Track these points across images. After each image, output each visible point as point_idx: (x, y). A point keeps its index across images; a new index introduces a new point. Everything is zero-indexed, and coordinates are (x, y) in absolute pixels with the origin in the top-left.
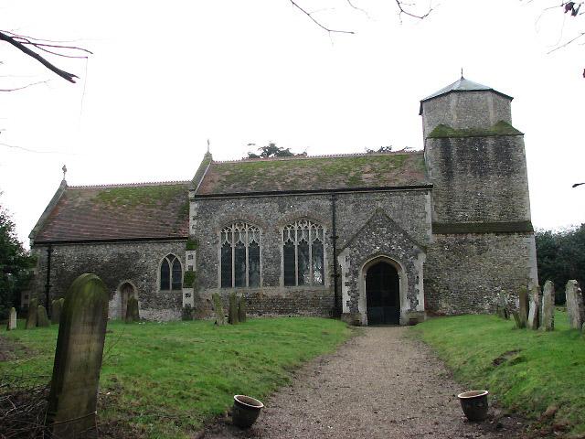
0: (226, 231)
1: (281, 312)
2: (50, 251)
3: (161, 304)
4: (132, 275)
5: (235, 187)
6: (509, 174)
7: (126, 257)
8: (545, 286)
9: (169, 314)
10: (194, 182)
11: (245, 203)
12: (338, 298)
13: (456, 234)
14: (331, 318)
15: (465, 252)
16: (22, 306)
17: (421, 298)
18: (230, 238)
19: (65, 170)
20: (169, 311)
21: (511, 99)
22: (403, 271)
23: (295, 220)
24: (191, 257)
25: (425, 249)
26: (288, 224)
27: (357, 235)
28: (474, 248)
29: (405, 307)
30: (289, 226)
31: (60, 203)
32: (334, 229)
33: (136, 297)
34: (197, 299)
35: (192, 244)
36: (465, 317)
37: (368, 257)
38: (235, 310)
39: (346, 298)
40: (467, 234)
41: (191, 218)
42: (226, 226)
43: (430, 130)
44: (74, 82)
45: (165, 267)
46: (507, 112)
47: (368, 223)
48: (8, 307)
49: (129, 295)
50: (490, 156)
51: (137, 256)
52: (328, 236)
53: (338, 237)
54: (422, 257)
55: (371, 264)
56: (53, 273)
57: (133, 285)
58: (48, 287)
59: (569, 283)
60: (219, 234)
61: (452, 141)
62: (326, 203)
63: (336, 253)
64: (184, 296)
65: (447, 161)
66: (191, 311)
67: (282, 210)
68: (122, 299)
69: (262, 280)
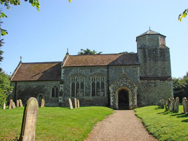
4: (42, 92)
12: (109, 100)
15: (150, 86)
17: (136, 101)
21: (165, 37)
24: (62, 86)
28: (153, 85)
29: (131, 103)
34: (64, 100)
39: (112, 101)
41: (62, 74)
45: (53, 89)
51: (44, 86)
53: (109, 81)
56: (17, 91)
61: (146, 50)
63: (108, 86)
64: (59, 99)
65: (145, 56)
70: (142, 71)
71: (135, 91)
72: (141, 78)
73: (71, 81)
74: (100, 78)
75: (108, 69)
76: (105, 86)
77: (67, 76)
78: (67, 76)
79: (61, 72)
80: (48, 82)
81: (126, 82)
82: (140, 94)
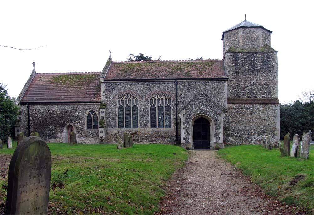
2: (29, 107)
3: (87, 136)
4: (72, 121)
6: (268, 73)
7: (69, 111)
11: (130, 85)
12: (178, 135)
14: (174, 145)
15: (243, 113)
16: (16, 135)
17: (221, 136)
18: (122, 103)
19: (34, 64)
22: (213, 122)
24: (103, 112)
25: (224, 111)
29: (213, 141)
32: (177, 100)
34: (107, 134)
35: (103, 106)
38: (127, 142)
39: (183, 135)
40: (245, 104)
42: (120, 96)
43: (227, 48)
45: (89, 116)
46: (268, 39)
47: (195, 97)
50: (259, 63)
51: (75, 111)
52: (174, 103)
53: (178, 104)
54: (223, 115)
55: (196, 118)
56: (31, 119)
57: (72, 125)
58: (29, 125)
60: (117, 100)
62: (173, 86)
64: (99, 132)
65: (236, 65)
66: (103, 139)
67: (149, 89)
70: (232, 88)
71: (221, 120)
74: (164, 98)
76: (172, 113)
81: (206, 106)
82: (228, 126)
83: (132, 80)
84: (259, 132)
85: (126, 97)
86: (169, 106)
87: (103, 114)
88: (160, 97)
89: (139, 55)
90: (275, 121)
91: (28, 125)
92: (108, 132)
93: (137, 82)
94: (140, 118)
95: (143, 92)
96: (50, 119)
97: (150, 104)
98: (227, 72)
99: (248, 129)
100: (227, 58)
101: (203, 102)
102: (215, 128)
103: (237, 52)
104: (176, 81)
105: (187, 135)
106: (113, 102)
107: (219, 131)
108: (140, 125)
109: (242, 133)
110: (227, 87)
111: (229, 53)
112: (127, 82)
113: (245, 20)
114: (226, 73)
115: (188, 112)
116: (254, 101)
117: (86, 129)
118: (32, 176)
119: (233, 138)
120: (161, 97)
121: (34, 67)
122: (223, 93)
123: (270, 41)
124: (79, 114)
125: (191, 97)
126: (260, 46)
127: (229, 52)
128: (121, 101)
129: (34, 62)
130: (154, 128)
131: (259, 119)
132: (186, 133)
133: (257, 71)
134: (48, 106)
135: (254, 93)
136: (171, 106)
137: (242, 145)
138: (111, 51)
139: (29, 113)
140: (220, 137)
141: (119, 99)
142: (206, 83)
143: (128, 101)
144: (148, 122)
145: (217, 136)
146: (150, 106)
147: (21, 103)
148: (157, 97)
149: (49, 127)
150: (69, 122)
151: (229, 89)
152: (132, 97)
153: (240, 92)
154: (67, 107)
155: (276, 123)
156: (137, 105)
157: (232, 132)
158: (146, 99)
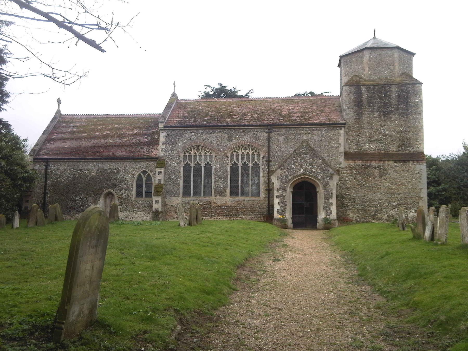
0: (187, 154)
1: (227, 216)
2: (47, 166)
3: (136, 208)
4: (113, 186)
5: (195, 120)
6: (408, 115)
7: (110, 171)
8: (441, 210)
9: (141, 216)
10: (163, 116)
11: (202, 133)
12: (270, 207)
13: (362, 161)
14: (264, 222)
15: (369, 175)
16: (23, 208)
17: (334, 209)
18: (190, 159)
19: (59, 101)
20: (142, 213)
21: (413, 54)
22: (321, 188)
23: (239, 147)
24: (160, 173)
25: (338, 172)
26: (234, 150)
27: (286, 160)
28: (376, 172)
29: (321, 216)
30: (235, 151)
31: (55, 128)
32: (269, 155)
33: (117, 202)
34: (164, 205)
35: (161, 163)
36: (368, 225)
37: (295, 177)
38: (194, 216)
39: (277, 207)
40: (371, 161)
41: (161, 144)
42: (187, 150)
43: (345, 80)
44: (103, 51)
45: (139, 179)
46: (410, 65)
47: (295, 151)
48: (14, 211)
49: (111, 202)
50: (393, 101)
51: (118, 171)
52: (264, 160)
53: (271, 161)
54: (336, 178)
55: (297, 182)
56: (49, 183)
57: (114, 193)
58: (45, 193)
59: (462, 209)
60: (182, 155)
61: (364, 89)
62: (263, 135)
63: (270, 173)
64: (154, 202)
65: (359, 103)
66: (159, 213)
67: (230, 139)
68: (105, 204)
69: (213, 191)
70: (351, 138)
71: (333, 185)
72: (347, 156)
73: (182, 159)
74: (251, 153)
75: (269, 133)
76: (261, 174)
77: (172, 149)
78: (172, 149)
79: (158, 139)
80: (127, 164)
81: (312, 164)
82: (345, 194)
83: (206, 126)
84: (394, 204)
85: (196, 151)
86: (258, 164)
87: (161, 175)
88: (245, 151)
89: (218, 87)
90: (420, 187)
91: (43, 193)
92: (167, 203)
93: (212, 129)
94: (215, 182)
95: (221, 143)
96: (80, 183)
97: (230, 162)
98: (345, 114)
99: (376, 198)
100: (345, 94)
101: (307, 159)
102: (323, 196)
103: (360, 85)
104: (269, 128)
105: (283, 207)
106: (176, 159)
107: (331, 201)
108: (215, 192)
109: (368, 205)
110: (344, 135)
111: (348, 87)
112: (198, 130)
113: (375, 37)
114: (342, 116)
115: (285, 172)
116: (388, 157)
117: (133, 199)
118: (91, 247)
119: (353, 212)
120: (247, 151)
121: (59, 105)
122: (338, 145)
123: (412, 67)
124: (124, 175)
125: (291, 151)
126: (396, 76)
127: (347, 86)
128: (188, 157)
129: (59, 99)
130: (235, 196)
131: (393, 183)
132: (282, 204)
133: (390, 113)
134: (78, 164)
135: (385, 145)
136: (261, 164)
137: (367, 222)
138: (175, 85)
139: (46, 174)
140: (331, 209)
141: (185, 153)
142: (313, 130)
143: (198, 157)
144: (227, 187)
145: (328, 209)
146: (230, 165)
147: (34, 159)
148: (240, 150)
149: (76, 196)
150: (108, 187)
151: (347, 139)
152: (205, 150)
153: (364, 143)
154: (107, 166)
155: (421, 189)
156: (212, 162)
157: (352, 202)
158: (225, 154)
